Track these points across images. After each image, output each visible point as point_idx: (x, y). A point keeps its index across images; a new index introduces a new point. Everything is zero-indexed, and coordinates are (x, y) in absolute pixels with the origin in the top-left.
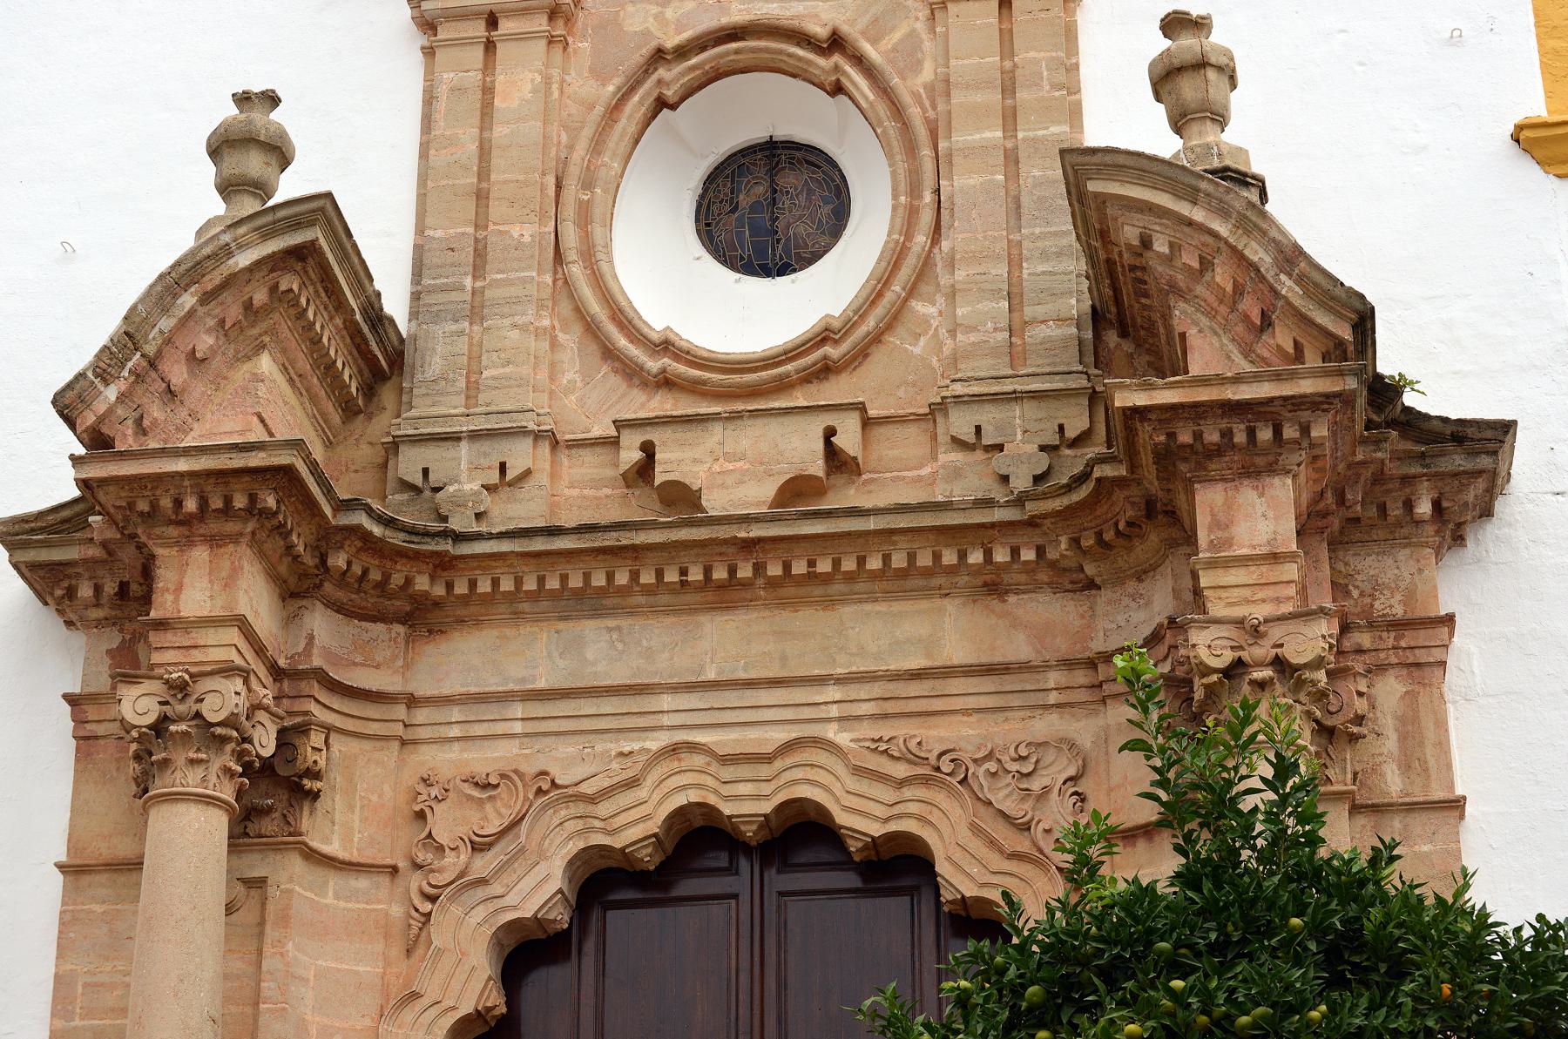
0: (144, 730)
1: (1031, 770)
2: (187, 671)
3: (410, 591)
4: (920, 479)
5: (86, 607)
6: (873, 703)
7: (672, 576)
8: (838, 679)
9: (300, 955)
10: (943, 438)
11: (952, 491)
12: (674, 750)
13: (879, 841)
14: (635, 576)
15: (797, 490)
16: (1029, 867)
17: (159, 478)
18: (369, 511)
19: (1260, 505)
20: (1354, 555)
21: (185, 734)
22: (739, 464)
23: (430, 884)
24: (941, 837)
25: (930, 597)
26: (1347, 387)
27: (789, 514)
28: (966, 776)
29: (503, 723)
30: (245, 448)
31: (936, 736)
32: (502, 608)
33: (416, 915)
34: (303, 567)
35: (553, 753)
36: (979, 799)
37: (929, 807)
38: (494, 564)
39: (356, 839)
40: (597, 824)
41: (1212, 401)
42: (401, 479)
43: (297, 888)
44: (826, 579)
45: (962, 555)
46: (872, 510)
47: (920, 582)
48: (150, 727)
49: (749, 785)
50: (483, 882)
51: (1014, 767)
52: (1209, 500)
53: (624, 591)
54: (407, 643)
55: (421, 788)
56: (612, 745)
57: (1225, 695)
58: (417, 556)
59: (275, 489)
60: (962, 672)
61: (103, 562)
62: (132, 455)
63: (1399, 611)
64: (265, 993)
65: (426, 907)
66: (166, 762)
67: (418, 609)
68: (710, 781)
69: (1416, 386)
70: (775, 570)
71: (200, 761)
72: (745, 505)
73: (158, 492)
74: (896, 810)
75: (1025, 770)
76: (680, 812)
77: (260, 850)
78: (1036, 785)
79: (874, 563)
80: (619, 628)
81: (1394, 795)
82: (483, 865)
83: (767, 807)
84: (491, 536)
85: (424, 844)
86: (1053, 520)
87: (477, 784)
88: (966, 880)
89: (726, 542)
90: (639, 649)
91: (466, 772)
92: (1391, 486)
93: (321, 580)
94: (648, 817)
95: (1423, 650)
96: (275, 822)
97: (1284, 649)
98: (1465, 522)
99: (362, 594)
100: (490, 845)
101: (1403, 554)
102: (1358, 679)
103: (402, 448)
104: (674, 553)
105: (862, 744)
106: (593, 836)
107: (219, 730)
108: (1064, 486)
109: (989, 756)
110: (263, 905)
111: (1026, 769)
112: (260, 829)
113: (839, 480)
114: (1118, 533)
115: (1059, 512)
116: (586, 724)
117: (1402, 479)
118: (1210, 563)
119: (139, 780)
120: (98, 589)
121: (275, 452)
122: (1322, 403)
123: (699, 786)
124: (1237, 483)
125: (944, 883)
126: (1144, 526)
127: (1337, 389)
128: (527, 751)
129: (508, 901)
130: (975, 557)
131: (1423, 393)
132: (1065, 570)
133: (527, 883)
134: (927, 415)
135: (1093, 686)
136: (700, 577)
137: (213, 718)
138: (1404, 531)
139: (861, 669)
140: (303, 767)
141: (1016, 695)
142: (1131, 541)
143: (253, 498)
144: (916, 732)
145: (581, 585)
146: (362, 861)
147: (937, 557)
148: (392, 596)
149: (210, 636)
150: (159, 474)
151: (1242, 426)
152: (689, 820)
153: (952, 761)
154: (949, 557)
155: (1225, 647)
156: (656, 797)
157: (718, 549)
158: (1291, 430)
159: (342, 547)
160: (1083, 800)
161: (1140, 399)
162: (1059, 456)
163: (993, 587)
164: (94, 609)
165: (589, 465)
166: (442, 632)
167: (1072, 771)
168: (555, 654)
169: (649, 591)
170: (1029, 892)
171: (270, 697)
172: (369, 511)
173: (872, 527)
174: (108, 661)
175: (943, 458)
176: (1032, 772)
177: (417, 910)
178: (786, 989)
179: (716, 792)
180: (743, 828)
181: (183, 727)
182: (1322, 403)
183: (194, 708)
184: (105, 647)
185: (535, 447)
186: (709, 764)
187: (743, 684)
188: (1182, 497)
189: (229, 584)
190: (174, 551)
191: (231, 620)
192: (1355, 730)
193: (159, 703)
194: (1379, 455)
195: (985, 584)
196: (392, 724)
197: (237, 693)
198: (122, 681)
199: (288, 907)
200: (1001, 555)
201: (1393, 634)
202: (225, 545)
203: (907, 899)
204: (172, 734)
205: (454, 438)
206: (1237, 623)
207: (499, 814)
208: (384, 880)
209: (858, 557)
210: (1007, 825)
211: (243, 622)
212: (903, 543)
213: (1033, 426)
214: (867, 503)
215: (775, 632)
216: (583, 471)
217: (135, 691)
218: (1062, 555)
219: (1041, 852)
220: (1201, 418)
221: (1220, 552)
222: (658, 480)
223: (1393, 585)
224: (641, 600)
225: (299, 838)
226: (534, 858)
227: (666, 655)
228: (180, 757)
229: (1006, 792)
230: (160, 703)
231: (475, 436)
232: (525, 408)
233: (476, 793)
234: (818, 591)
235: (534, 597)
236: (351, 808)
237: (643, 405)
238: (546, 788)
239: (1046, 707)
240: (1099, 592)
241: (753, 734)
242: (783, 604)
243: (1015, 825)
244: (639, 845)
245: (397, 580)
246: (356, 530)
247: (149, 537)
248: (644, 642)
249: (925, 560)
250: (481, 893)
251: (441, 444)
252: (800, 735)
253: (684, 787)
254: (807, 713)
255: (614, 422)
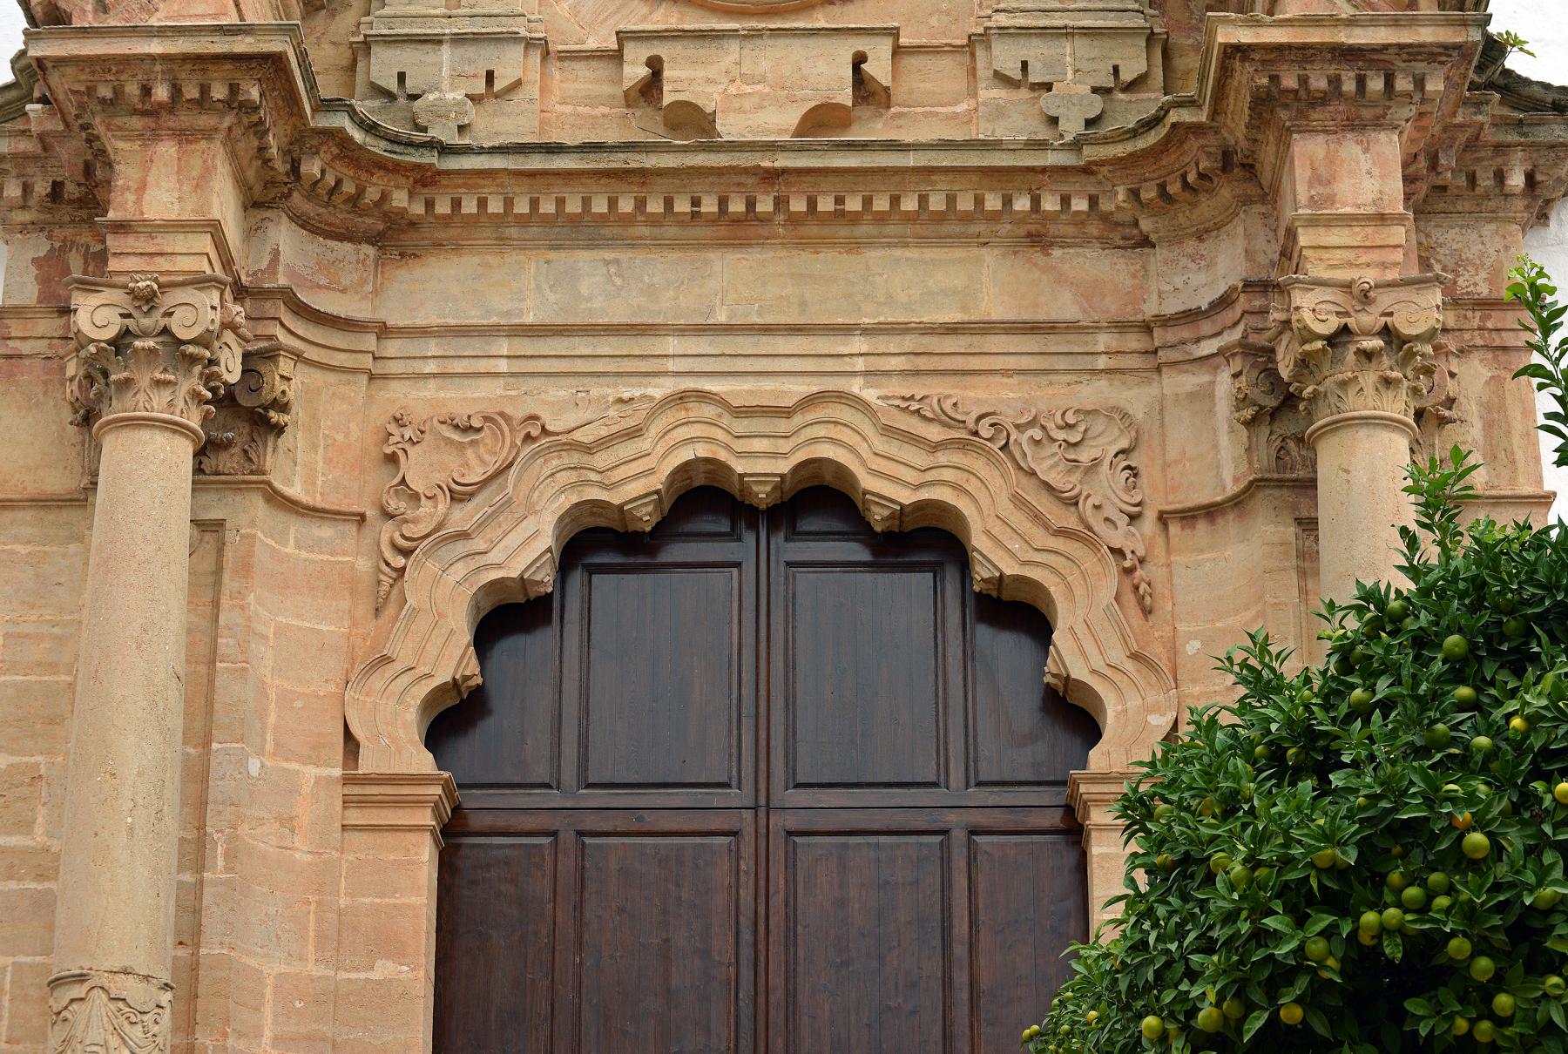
0: (103, 345)
1: (1078, 439)
2: (156, 280)
3: (386, 207)
4: (955, 116)
5: (11, 209)
6: (903, 358)
7: (682, 206)
8: (866, 329)
9: (260, 610)
10: (983, 72)
11: (993, 131)
12: (681, 398)
13: (908, 510)
14: (641, 204)
15: (821, 119)
16: (1077, 545)
17: (126, 61)
18: (352, 113)
19: (1365, 162)
20: (1436, 226)
21: (151, 351)
22: (758, 87)
23: (403, 536)
24: (979, 508)
25: (967, 245)
26: (1470, 39)
27: (820, 143)
28: (1007, 443)
29: (486, 360)
30: (229, 30)
31: (973, 398)
32: (487, 233)
33: (387, 570)
34: (272, 173)
35: (543, 396)
36: (1021, 468)
37: (966, 474)
38: (482, 182)
39: (319, 483)
40: (593, 476)
41: (1323, 44)
42: (372, 83)
43: (259, 533)
44: (854, 219)
45: (1007, 201)
46: (913, 145)
47: (958, 229)
48: (110, 342)
49: (765, 441)
50: (464, 535)
51: (1060, 435)
52: (1308, 150)
53: (626, 220)
54: (376, 266)
55: (393, 428)
56: (609, 391)
57: (1326, 366)
58: (396, 168)
59: (259, 80)
60: (1004, 328)
61: (36, 158)
62: (97, 32)
63: (1484, 290)
64: (222, 650)
65: (399, 561)
66: (127, 383)
67: (390, 228)
68: (720, 435)
69: (1526, 47)
70: (798, 205)
71: (168, 383)
72: (766, 131)
73: (123, 77)
74: (929, 476)
75: (1072, 440)
76: (685, 468)
77: (217, 489)
78: (1085, 456)
79: (909, 204)
80: (617, 262)
81: (1479, 486)
82: (461, 518)
83: (784, 467)
84: (481, 151)
85: (396, 491)
86: (1111, 168)
87: (457, 427)
88: (1006, 557)
89: (746, 171)
90: (640, 285)
91: (444, 413)
92: (1482, 154)
93: (290, 189)
94: (650, 472)
95: (1510, 333)
96: (236, 459)
97: (1394, 318)
98: (1553, 200)
99: (331, 209)
100: (471, 495)
101: (1488, 229)
102: (1451, 358)
103: (375, 49)
104: (686, 181)
105: (891, 402)
106: (588, 489)
107: (191, 349)
108: (1128, 131)
109: (1032, 423)
110: (220, 551)
111: (1074, 437)
112: (218, 466)
113: (865, 112)
114: (1186, 185)
115: (1121, 159)
116: (580, 366)
117: (1495, 147)
118: (1311, 220)
119: (77, 405)
120: (27, 189)
121: (266, 38)
122: (1440, 54)
123: (709, 440)
124: (1339, 136)
125: (980, 558)
126: (1216, 180)
127: (1459, 40)
128: (513, 393)
129: (493, 557)
130: (1022, 204)
131: (1533, 55)
132: (1117, 224)
133: (514, 539)
134: (963, 46)
135: (1147, 352)
136: (715, 209)
137: (183, 334)
138: (1492, 204)
139: (890, 320)
140: (270, 397)
141: (1061, 357)
142: (1196, 195)
143: (234, 89)
144: (952, 392)
145: (580, 210)
146: (327, 507)
147: (979, 201)
148: (363, 213)
149: (178, 243)
150: (128, 55)
151: (1352, 74)
152: (690, 478)
153: (992, 425)
154: (993, 202)
155: (1328, 313)
156: (660, 450)
157: (737, 179)
158: (1404, 81)
159: (317, 153)
160: (1135, 476)
161: (1246, 36)
162: (1112, 100)
163: (1038, 238)
164: (19, 212)
165: (585, 81)
166: (415, 256)
167: (1124, 443)
168: (545, 286)
169: (654, 221)
170: (1077, 572)
171: (243, 314)
172: (352, 113)
173: (912, 164)
174: (33, 271)
175: (983, 94)
176: (1082, 439)
177: (388, 564)
178: (794, 668)
179: (727, 447)
180: (755, 488)
181: (150, 343)
182: (1440, 54)
183: (162, 323)
184: (31, 255)
185: (526, 55)
186: (720, 416)
187: (760, 330)
188: (1271, 148)
189: (201, 184)
190: (136, 146)
191: (203, 226)
192: (1447, 413)
193: (121, 315)
194: (1480, 118)
195: (1029, 235)
196: (360, 356)
197: (213, 308)
198: (78, 289)
199: (250, 554)
200: (1050, 204)
201: (1478, 314)
202: (197, 141)
203: (930, 576)
204: (136, 350)
205: (435, 41)
206: (1342, 286)
207: (482, 461)
208: (351, 529)
209: (891, 197)
210: (1051, 499)
211: (217, 229)
212: (942, 183)
213: (1085, 66)
214: (907, 138)
215: (793, 274)
216: (577, 86)
217: (94, 300)
218: (1118, 208)
219: (1090, 529)
220: (1307, 62)
221: (1322, 209)
222: (667, 100)
223: (1478, 262)
224: (645, 231)
225: (264, 477)
226: (522, 511)
227: (671, 293)
228: (144, 379)
229: (1050, 462)
230: (123, 316)
231: (459, 39)
232: (515, 12)
233: (456, 436)
234: (844, 231)
235: (523, 221)
236: (314, 447)
237: (644, 18)
238: (535, 432)
239: (1094, 372)
240: (1152, 250)
241: (768, 385)
242: (803, 244)
243: (1060, 499)
244: (639, 502)
245: (372, 194)
246: (337, 137)
247: (108, 129)
248: (646, 279)
249: (965, 204)
250: (461, 547)
251: (419, 46)
252: (823, 388)
253: (691, 440)
254: (830, 365)
255: (617, 33)
